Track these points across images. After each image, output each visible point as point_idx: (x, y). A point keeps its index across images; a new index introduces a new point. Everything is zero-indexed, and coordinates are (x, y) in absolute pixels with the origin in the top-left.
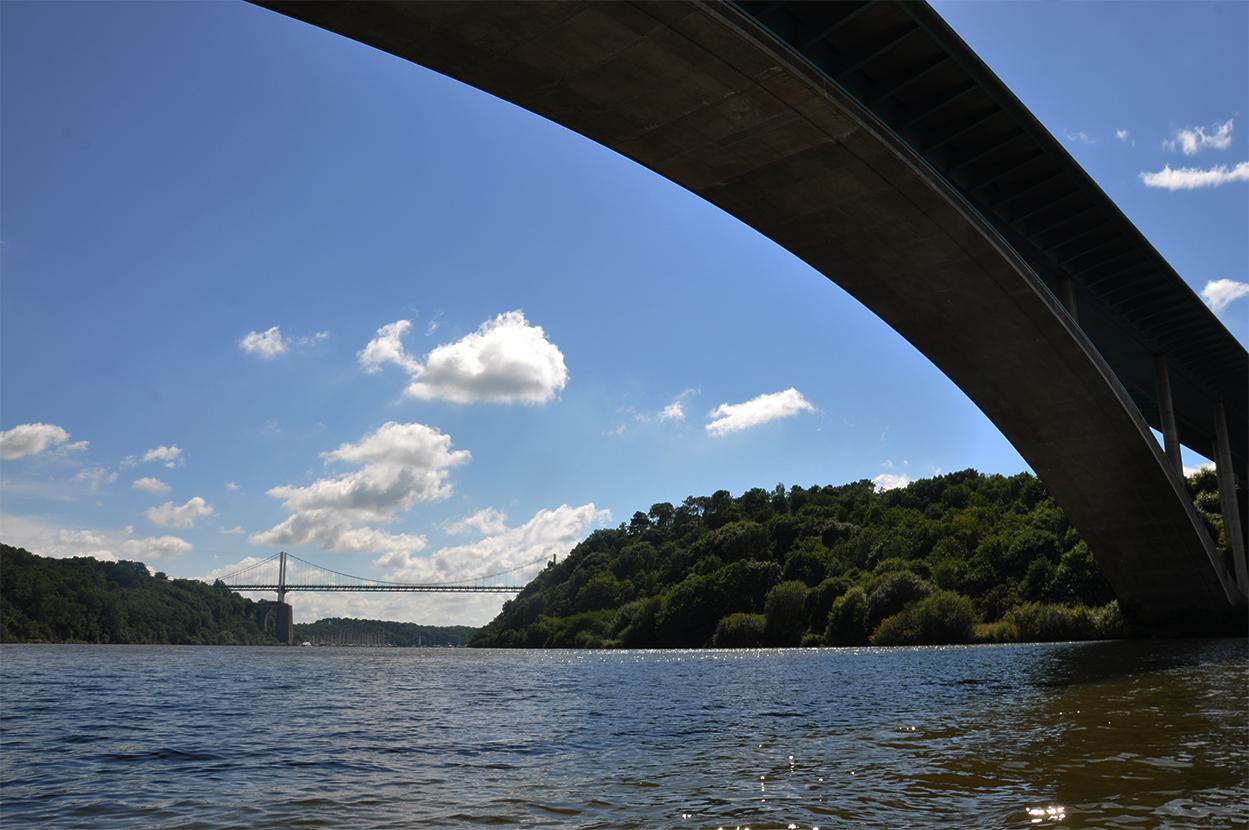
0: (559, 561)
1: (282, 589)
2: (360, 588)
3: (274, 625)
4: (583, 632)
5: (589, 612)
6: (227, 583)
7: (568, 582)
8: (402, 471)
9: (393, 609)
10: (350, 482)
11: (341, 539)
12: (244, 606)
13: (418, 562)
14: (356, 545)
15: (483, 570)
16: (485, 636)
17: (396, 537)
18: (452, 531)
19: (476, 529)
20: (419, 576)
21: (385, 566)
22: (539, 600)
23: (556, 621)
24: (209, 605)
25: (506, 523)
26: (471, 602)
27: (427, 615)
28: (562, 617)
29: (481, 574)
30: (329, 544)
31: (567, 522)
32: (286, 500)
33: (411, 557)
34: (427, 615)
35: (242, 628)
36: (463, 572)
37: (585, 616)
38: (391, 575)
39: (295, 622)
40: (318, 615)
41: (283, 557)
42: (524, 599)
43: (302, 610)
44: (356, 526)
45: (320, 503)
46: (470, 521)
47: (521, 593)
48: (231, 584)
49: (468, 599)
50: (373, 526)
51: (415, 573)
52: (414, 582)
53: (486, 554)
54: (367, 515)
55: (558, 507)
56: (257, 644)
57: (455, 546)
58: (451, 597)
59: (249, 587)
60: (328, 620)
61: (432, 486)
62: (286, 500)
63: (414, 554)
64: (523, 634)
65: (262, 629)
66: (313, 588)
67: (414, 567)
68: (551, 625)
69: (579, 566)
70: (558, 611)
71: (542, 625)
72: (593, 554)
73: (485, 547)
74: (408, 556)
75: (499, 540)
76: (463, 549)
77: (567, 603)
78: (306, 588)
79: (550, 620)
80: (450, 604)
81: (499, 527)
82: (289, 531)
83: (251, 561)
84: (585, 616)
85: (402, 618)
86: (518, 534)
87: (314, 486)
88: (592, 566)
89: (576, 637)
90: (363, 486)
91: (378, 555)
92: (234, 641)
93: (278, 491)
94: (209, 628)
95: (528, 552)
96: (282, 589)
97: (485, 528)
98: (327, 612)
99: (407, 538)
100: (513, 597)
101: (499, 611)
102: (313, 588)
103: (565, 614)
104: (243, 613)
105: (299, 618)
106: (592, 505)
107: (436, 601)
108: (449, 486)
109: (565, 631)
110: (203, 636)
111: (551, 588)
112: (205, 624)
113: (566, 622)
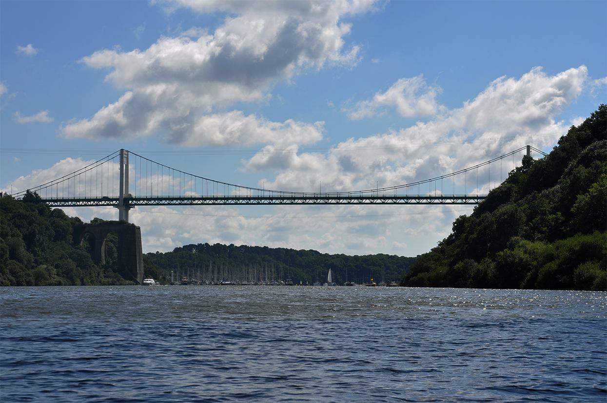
0: (536, 157)
1: (125, 203)
2: (226, 200)
3: (116, 255)
4: (589, 265)
5: (597, 232)
6: (43, 195)
7: (557, 187)
8: (342, 38)
9: (280, 231)
10: (207, 44)
11: (197, 129)
12: (71, 230)
13: (309, 159)
14: (218, 137)
15: (408, 171)
16: (427, 270)
17: (277, 125)
18: (361, 112)
19: (392, 108)
20: (313, 182)
21: (259, 167)
22: (512, 215)
23: (539, 246)
24: (19, 227)
25: (440, 100)
26: (393, 219)
27: (331, 238)
28: (551, 241)
29: (407, 178)
30: (178, 137)
31: (538, 96)
32: (113, 69)
33: (299, 153)
34: (331, 238)
35: (70, 260)
36: (380, 175)
37: (588, 239)
38: (272, 180)
39: (145, 251)
40: (174, 241)
41: (123, 156)
42: (488, 214)
43: (151, 233)
44: (218, 110)
45: (159, 74)
46: (380, 98)
47: (481, 205)
48: (49, 197)
49: (390, 215)
50: (245, 109)
51: (309, 176)
52: (309, 191)
53: (412, 147)
54: (230, 91)
55: (528, 71)
56: (92, 283)
57: (366, 137)
58: (363, 213)
59: (75, 202)
60: (190, 247)
61: (331, 49)
62: (113, 69)
63: (303, 149)
64: (489, 266)
65: (97, 260)
66: (170, 201)
67: (305, 168)
68: (532, 253)
69: (575, 162)
70: (542, 232)
71: (519, 253)
72: (598, 143)
73: (412, 138)
74: (296, 151)
75: (432, 126)
76: (376, 140)
77: (558, 219)
78: (158, 201)
79: (530, 245)
80: (364, 222)
81: (427, 105)
82: (121, 119)
83: (68, 164)
84: (588, 239)
85: (295, 244)
86: (459, 118)
87: (153, 48)
88: (598, 162)
89: (577, 272)
90: (227, 48)
91: (258, 148)
92: (58, 279)
93: (100, 58)
94: (20, 261)
95: (477, 142)
96: (125, 203)
97: (406, 108)
98: (186, 235)
99: (296, 127)
100: (468, 211)
101: (447, 232)
102: (170, 201)
103: (554, 234)
104: (70, 237)
105: (149, 246)
106: (583, 68)
107: (342, 218)
108: (356, 49)
109: (558, 262)
110: (13, 273)
111: (529, 197)
112: (14, 255)
113: (557, 248)
